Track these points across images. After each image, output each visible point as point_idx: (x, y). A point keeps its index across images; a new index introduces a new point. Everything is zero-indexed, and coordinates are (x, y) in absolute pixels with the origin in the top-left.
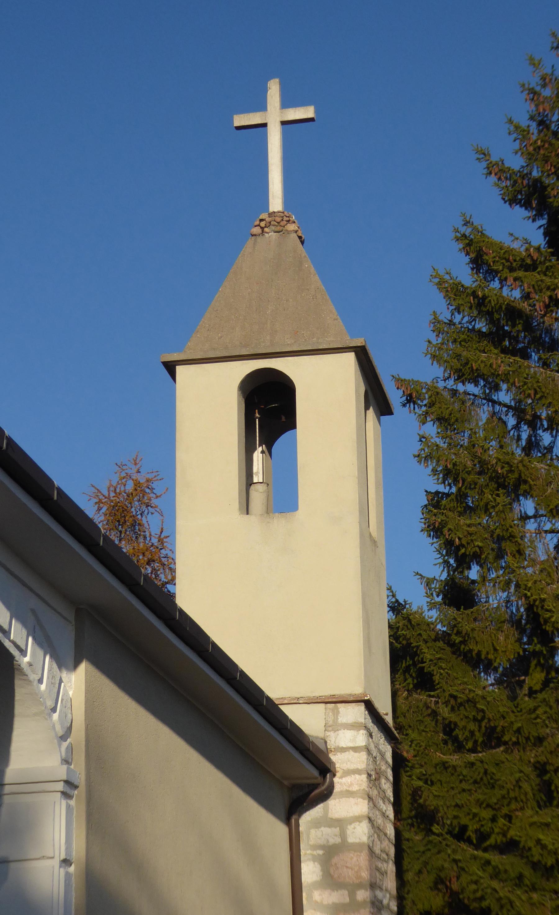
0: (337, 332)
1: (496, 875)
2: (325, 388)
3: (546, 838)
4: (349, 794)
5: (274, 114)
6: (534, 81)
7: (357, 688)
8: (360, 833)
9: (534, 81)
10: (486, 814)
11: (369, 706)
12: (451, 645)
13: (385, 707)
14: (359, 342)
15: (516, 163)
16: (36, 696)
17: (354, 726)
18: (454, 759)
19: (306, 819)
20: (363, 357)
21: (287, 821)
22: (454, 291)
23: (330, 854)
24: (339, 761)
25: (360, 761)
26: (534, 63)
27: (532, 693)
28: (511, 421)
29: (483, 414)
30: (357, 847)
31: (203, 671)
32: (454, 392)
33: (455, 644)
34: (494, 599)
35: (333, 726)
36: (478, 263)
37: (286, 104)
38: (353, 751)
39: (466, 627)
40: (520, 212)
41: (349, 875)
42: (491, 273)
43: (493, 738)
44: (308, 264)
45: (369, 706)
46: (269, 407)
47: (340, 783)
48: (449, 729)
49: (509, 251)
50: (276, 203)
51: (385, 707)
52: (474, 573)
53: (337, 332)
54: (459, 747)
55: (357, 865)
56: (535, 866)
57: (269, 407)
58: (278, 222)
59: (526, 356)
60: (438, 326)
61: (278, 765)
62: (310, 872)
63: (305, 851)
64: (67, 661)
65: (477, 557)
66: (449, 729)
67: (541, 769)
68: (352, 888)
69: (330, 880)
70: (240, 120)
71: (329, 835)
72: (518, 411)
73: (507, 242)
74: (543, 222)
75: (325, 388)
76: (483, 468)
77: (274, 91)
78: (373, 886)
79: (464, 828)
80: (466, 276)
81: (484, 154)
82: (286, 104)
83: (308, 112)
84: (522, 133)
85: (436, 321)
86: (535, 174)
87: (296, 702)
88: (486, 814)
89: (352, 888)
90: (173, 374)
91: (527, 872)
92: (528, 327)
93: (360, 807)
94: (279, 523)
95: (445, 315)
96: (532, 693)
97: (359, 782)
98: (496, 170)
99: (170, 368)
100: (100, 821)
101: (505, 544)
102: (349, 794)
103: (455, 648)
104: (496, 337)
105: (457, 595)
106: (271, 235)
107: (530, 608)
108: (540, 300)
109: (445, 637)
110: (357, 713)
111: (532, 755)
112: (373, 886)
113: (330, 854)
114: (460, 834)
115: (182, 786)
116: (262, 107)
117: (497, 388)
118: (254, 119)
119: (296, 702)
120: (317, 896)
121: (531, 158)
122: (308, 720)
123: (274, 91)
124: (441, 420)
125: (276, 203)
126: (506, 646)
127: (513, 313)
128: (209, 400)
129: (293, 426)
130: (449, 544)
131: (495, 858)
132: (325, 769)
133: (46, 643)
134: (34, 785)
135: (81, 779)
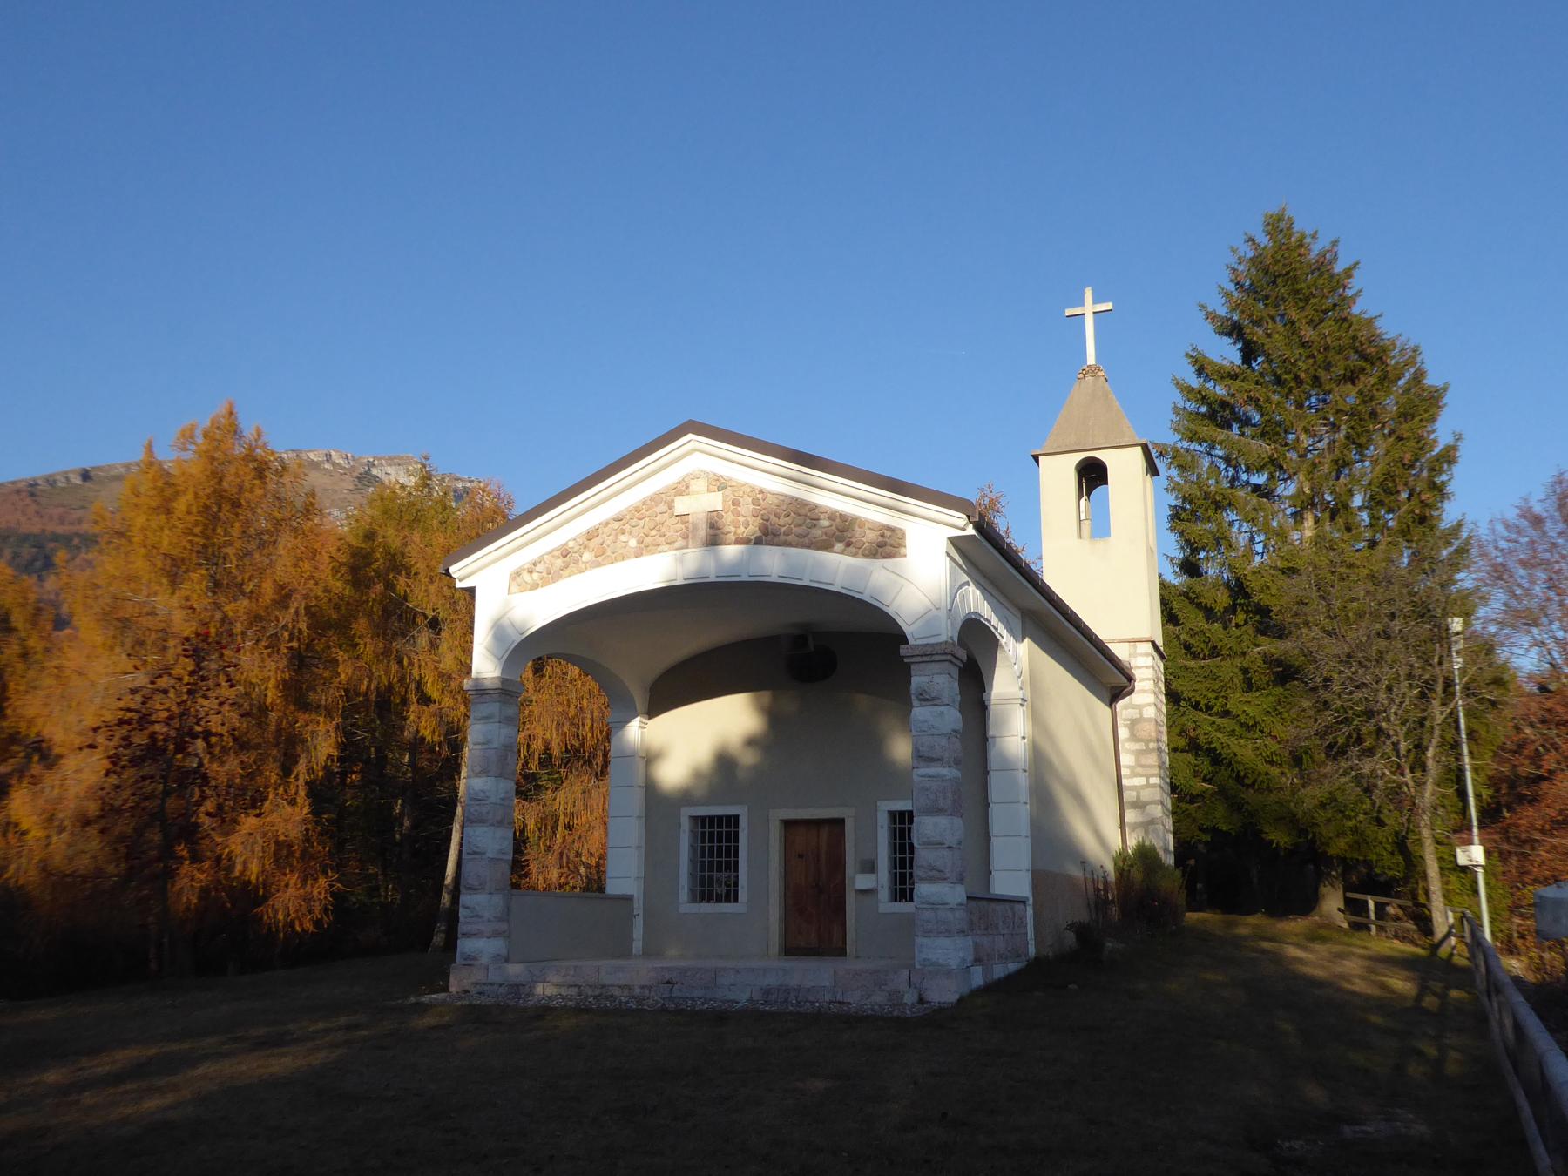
0: (1130, 435)
1: (1219, 729)
2: (1125, 466)
3: (1248, 709)
4: (1144, 691)
5: (1089, 308)
6: (1233, 262)
7: (1146, 635)
8: (1150, 712)
9: (1233, 262)
10: (1212, 695)
11: (1154, 643)
12: (1188, 597)
13: (1160, 643)
14: (1143, 441)
15: (1223, 311)
16: (1007, 658)
17: (1147, 655)
18: (1192, 664)
19: (1120, 705)
20: (1145, 448)
21: (1110, 705)
22: (1187, 391)
23: (1133, 724)
24: (1137, 673)
25: (1150, 673)
26: (1234, 250)
27: (1237, 626)
28: (1223, 466)
29: (1205, 463)
30: (1149, 720)
31: (1552, 1031)
32: (1188, 450)
33: (1188, 596)
34: (1211, 570)
35: (1134, 655)
36: (1200, 371)
37: (1095, 302)
38: (1146, 670)
39: (1198, 589)
40: (1227, 340)
41: (1144, 735)
42: (1208, 379)
43: (1215, 652)
44: (1112, 395)
45: (1154, 643)
46: (1092, 475)
47: (1138, 685)
48: (1187, 647)
49: (1221, 366)
50: (1091, 359)
51: (1160, 643)
52: (1202, 555)
53: (1130, 435)
54: (1195, 656)
55: (1148, 730)
56: (1242, 725)
57: (1092, 475)
58: (1093, 371)
59: (1230, 427)
60: (1176, 410)
61: (1105, 676)
62: (1123, 733)
63: (1120, 722)
64: (1020, 638)
65: (1203, 549)
66: (1187, 647)
67: (1245, 671)
68: (1147, 742)
69: (1134, 737)
70: (1069, 312)
71: (1134, 713)
72: (1227, 460)
73: (1219, 361)
74: (1239, 346)
75: (1125, 466)
76: (1207, 496)
77: (1088, 293)
78: (1158, 740)
79: (1198, 703)
80: (1194, 382)
81: (1204, 307)
82: (1095, 302)
83: (1109, 306)
84: (1228, 295)
85: (1175, 407)
86: (1236, 318)
87: (1113, 641)
88: (1212, 695)
89: (1147, 742)
90: (1037, 461)
91: (1237, 728)
92: (1233, 412)
93: (1151, 698)
94: (1100, 543)
95: (1181, 404)
96: (1237, 626)
97: (1150, 685)
98: (1211, 317)
99: (1036, 458)
100: (1037, 718)
101: (1221, 540)
102: (1144, 691)
103: (1191, 601)
104: (1211, 416)
105: (1190, 567)
106: (1089, 378)
107: (1238, 579)
108: (1241, 398)
109: (1185, 594)
110: (1148, 648)
111: (1238, 661)
112: (1158, 740)
113: (1133, 724)
114: (1196, 706)
115: (1067, 692)
116: (1082, 304)
117: (1213, 448)
118: (1077, 311)
119: (1113, 641)
120: (1127, 745)
121: (1233, 310)
122: (1120, 651)
123: (1088, 293)
124: (1179, 466)
125: (1091, 359)
126: (1222, 599)
127: (1224, 404)
128: (1059, 473)
129: (1106, 483)
130: (1187, 541)
131: (1218, 720)
132: (1130, 679)
133: (1011, 632)
134: (1006, 700)
135: (1028, 697)
